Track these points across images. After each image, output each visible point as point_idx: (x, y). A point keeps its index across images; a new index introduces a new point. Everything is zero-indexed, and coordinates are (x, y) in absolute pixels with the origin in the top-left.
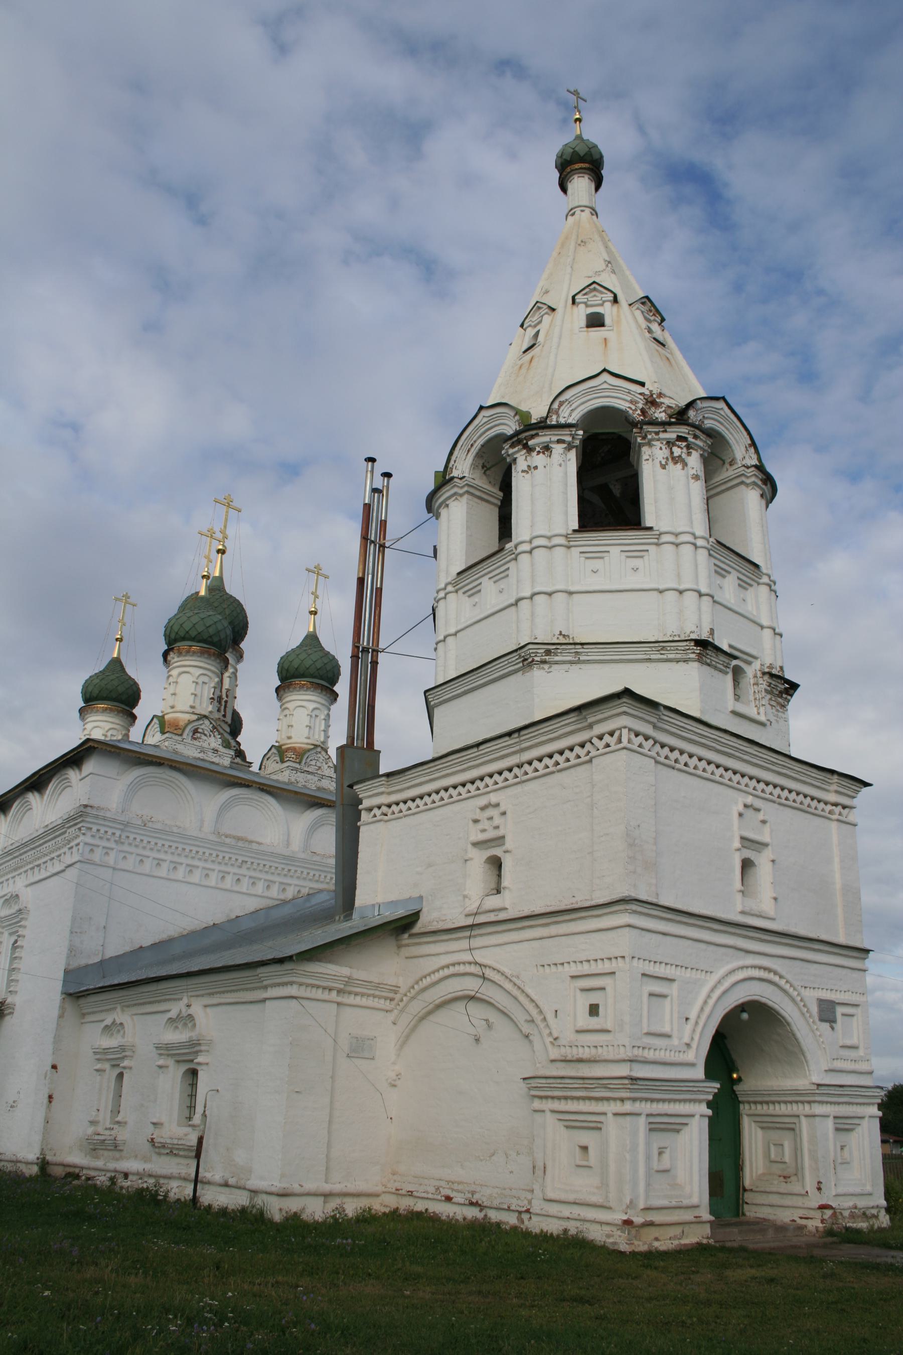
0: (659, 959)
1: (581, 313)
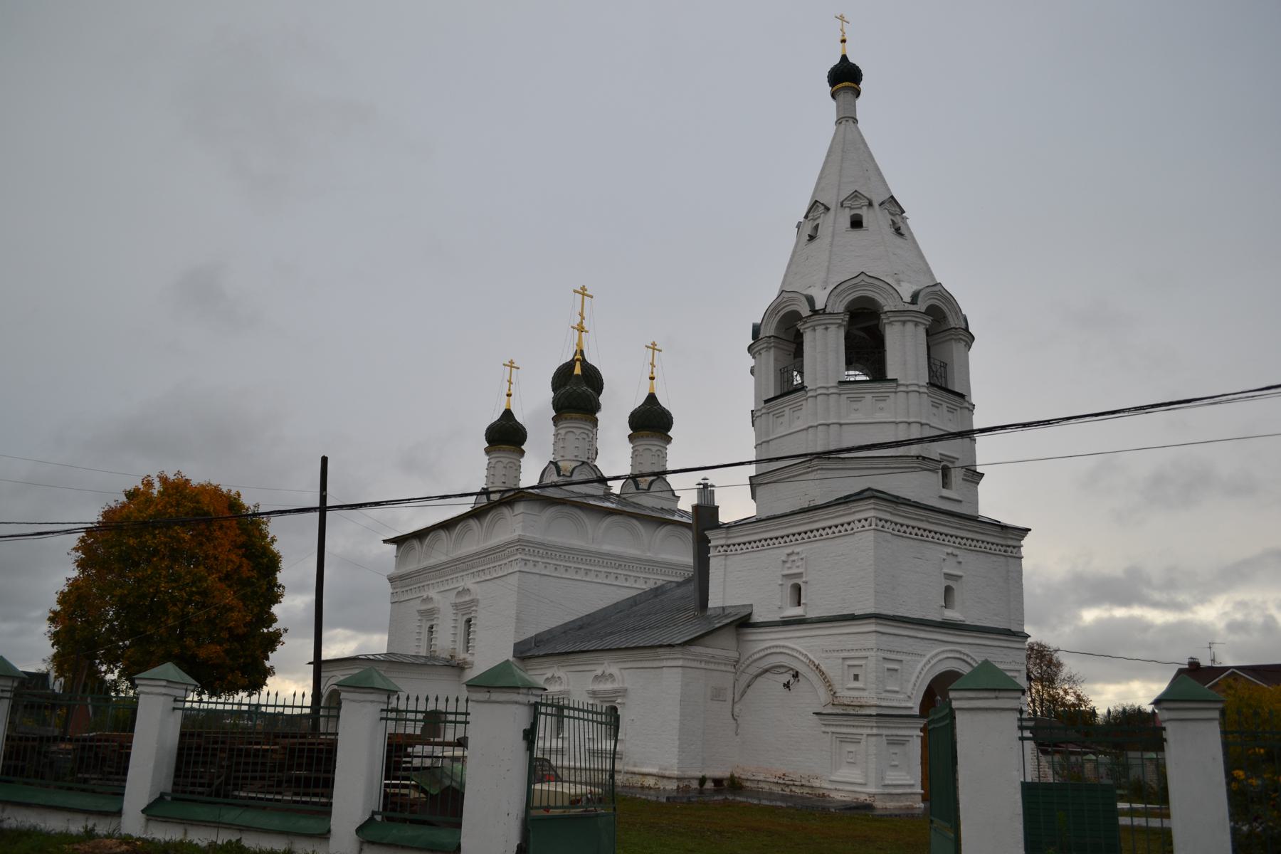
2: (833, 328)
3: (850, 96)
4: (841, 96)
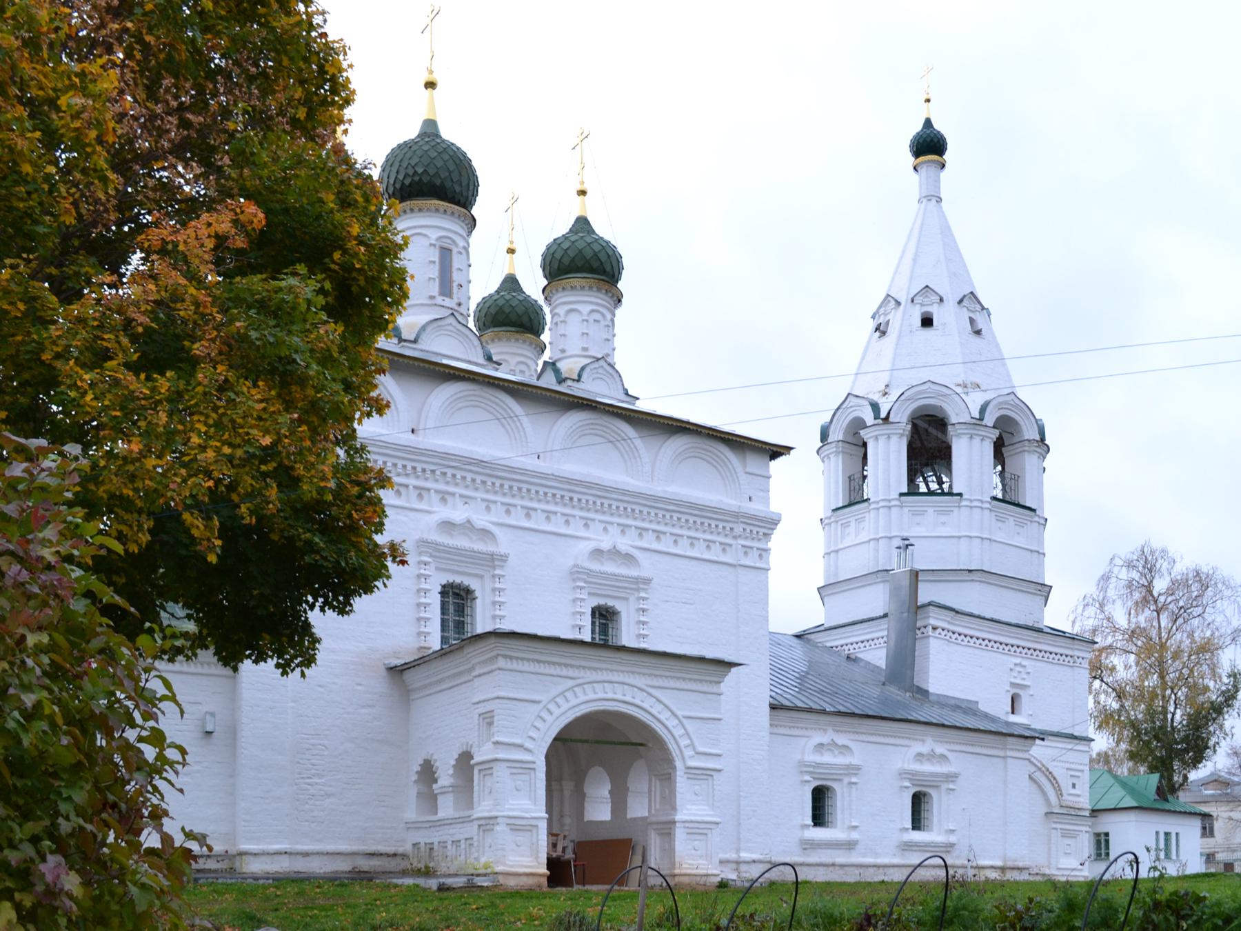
2: (894, 439)
3: (932, 170)
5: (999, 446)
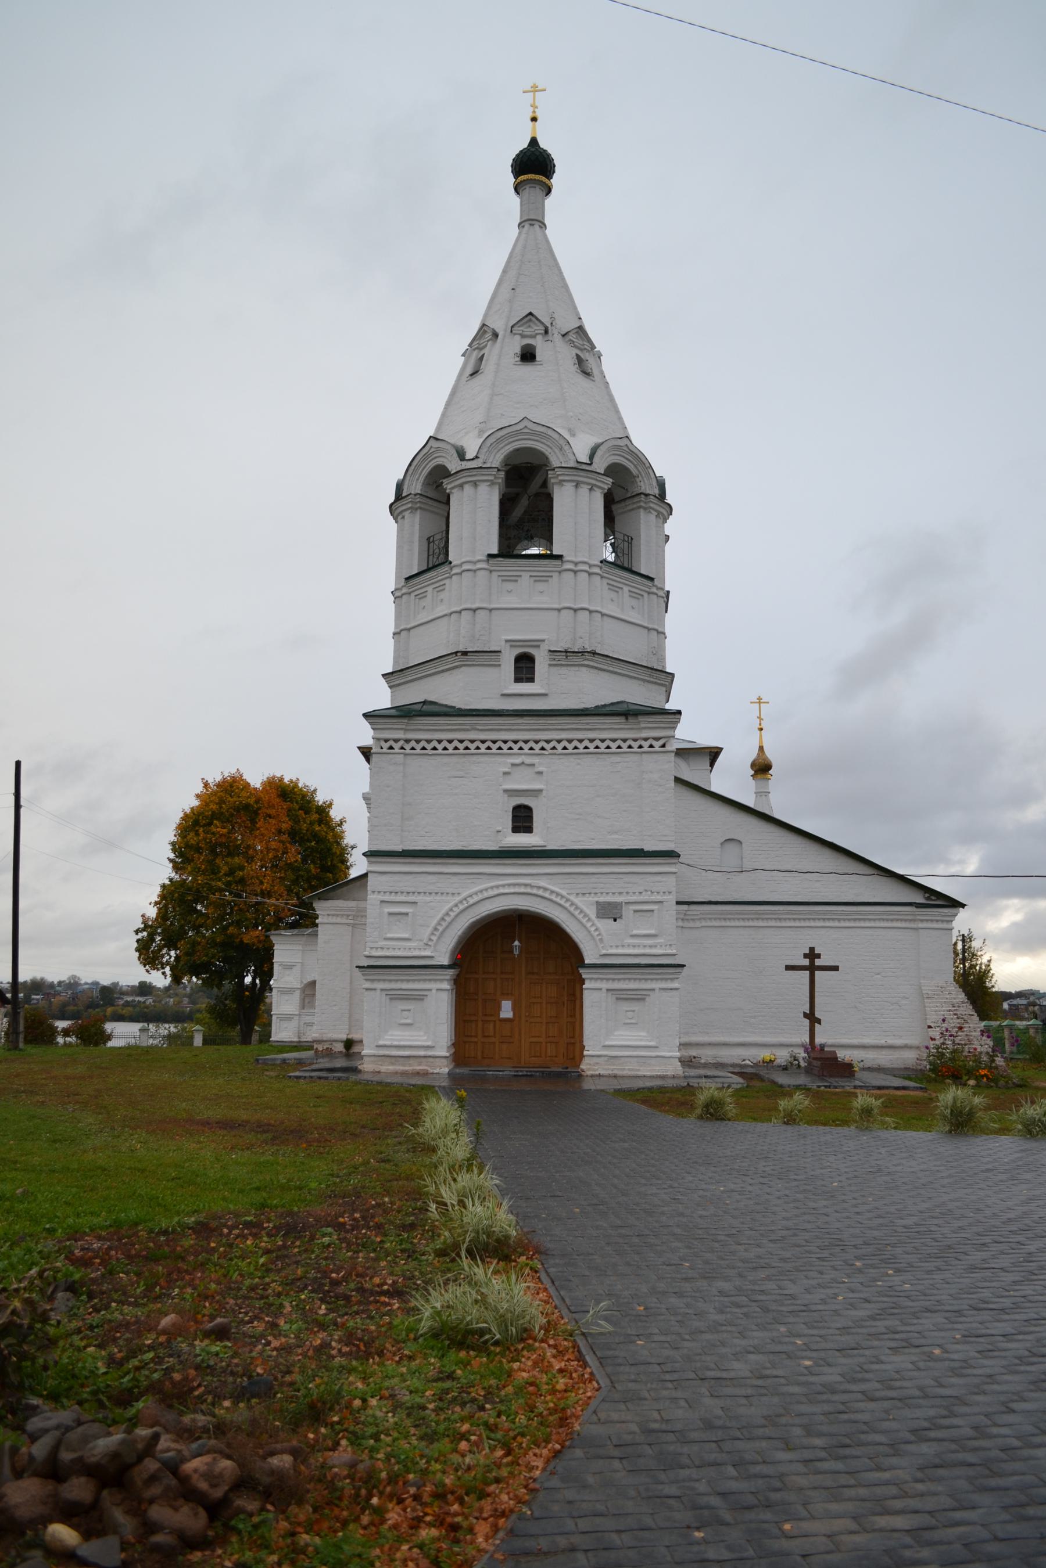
0: (398, 890)
1: (515, 345)
2: (483, 488)
3: (538, 192)
4: (527, 191)
5: (609, 501)
